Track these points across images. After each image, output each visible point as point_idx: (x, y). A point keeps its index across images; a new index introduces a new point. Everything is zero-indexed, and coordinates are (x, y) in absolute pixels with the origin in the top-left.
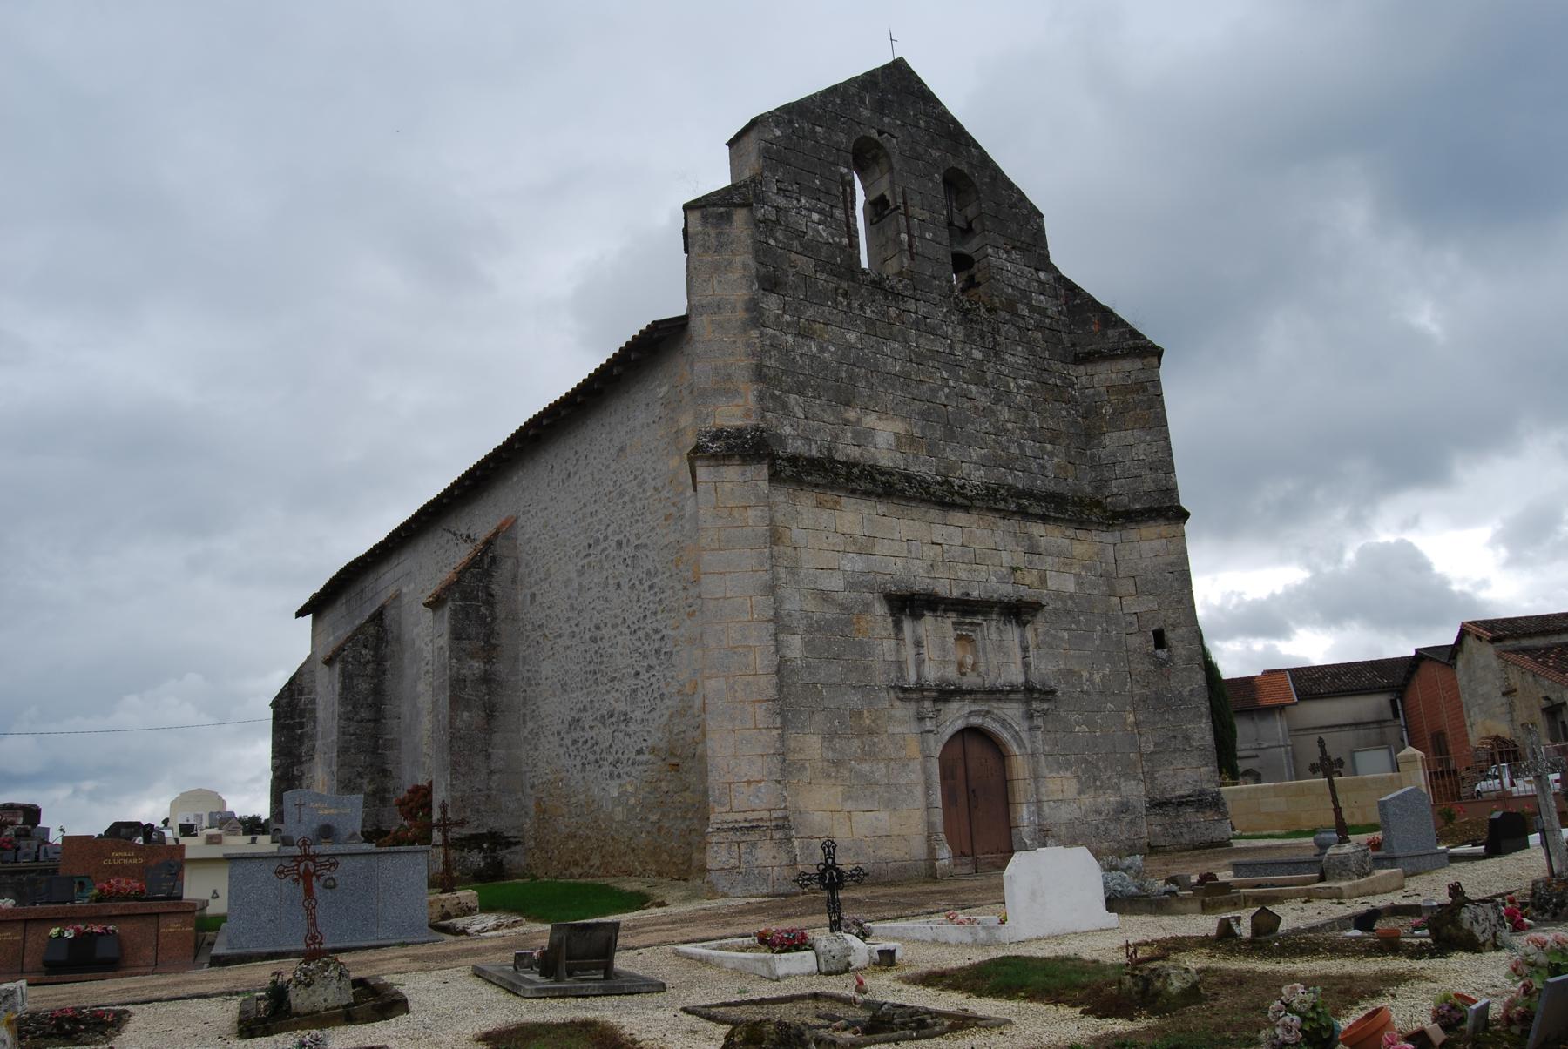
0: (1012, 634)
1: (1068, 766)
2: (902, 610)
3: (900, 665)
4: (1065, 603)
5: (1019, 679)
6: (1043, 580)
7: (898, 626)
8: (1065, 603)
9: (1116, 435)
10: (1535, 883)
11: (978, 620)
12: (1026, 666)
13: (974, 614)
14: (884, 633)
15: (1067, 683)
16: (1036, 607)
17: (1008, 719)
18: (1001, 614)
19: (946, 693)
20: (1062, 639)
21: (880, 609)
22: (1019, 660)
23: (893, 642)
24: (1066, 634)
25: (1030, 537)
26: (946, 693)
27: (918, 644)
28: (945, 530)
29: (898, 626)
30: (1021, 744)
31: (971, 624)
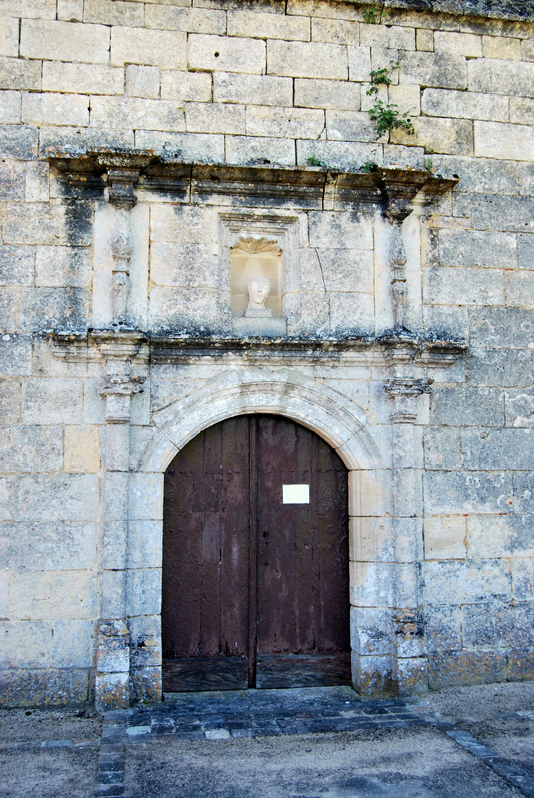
0: (373, 229)
1: (487, 492)
2: (94, 188)
3: (73, 295)
4: (514, 180)
5: (383, 322)
6: (466, 137)
7: (79, 221)
8: (514, 180)
9: (191, 646)
10: (91, 225)
11: (289, 209)
12: (397, 296)
13: (280, 198)
14: (42, 235)
15: (503, 332)
16: (436, 187)
17: (336, 403)
18: (345, 198)
19: (167, 347)
20: (502, 250)
21: (42, 191)
22: (382, 287)
23: (63, 253)
24: (512, 241)
25: (439, 59)
26: (167, 347)
27: (122, 253)
28: (222, 45)
29: (79, 221)
30: (371, 449)
31: (273, 219)
